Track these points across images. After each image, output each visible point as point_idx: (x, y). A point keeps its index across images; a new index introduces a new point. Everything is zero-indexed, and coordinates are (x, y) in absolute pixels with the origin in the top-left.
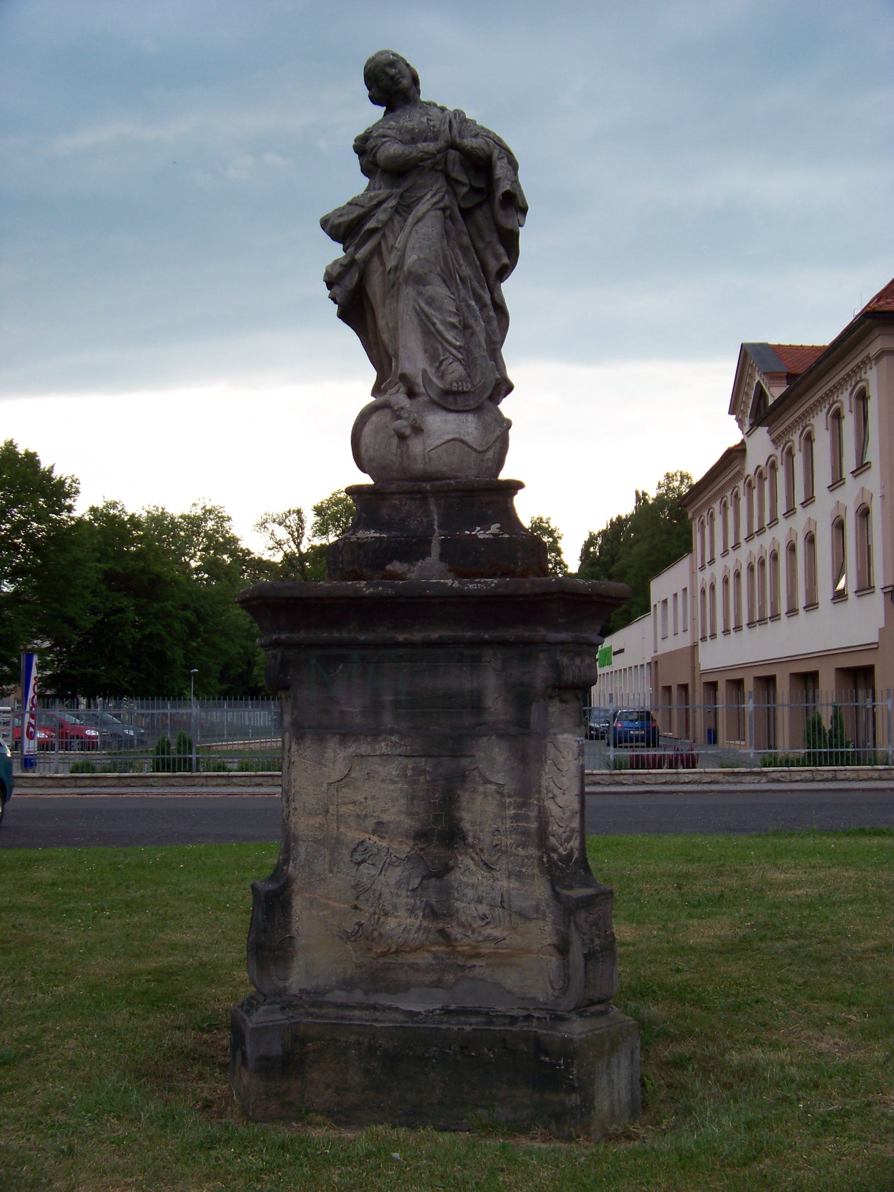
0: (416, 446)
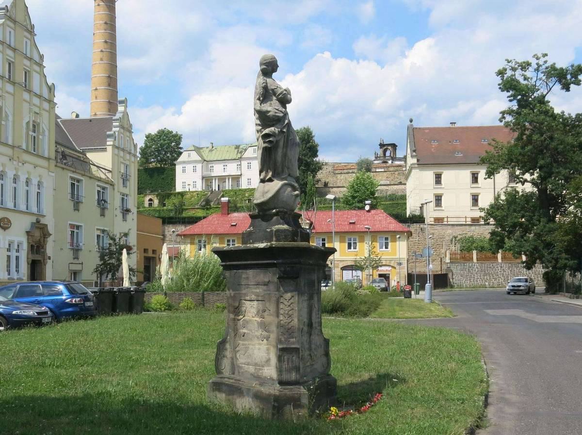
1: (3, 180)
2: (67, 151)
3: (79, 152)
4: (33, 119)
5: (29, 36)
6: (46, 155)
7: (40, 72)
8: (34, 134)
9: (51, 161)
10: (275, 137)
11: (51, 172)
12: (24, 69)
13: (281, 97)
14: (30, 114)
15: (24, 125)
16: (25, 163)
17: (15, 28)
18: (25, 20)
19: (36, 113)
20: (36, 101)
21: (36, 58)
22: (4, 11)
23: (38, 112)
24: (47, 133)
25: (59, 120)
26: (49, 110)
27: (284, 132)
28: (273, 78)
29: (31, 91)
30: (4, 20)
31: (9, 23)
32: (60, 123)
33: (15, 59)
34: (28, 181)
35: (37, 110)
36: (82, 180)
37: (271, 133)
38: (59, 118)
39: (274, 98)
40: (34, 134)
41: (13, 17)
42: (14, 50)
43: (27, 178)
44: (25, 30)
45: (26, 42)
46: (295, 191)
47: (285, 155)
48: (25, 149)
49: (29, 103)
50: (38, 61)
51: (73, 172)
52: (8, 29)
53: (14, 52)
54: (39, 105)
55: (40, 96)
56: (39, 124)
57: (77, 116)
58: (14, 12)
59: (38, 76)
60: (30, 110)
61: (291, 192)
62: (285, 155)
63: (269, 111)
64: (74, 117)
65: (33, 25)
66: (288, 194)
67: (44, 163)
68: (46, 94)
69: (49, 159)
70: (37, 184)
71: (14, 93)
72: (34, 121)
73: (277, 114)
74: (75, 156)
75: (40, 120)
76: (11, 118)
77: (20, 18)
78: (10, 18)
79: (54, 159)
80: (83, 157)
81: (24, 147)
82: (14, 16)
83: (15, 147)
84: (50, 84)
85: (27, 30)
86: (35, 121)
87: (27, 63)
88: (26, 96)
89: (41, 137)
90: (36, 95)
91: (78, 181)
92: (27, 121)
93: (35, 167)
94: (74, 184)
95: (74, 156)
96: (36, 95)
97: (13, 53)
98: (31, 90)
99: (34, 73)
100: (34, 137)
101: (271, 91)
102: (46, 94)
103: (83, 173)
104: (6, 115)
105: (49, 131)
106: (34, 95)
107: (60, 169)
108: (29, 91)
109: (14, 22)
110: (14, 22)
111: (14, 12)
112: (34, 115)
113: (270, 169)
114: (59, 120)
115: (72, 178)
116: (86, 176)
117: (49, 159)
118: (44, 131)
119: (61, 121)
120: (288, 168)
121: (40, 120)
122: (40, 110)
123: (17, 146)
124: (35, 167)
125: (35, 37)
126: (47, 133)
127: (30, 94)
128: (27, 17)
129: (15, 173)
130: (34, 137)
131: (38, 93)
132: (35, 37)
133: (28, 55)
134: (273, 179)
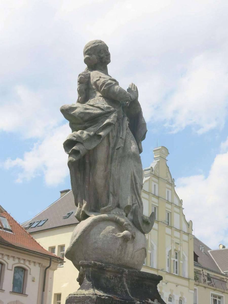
0: (130, 247)
1: (171, 301)
2: (212, 274)
3: (222, 274)
4: (175, 248)
5: (170, 187)
6: (187, 276)
7: (180, 212)
8: (176, 260)
9: (190, 281)
10: (82, 143)
11: (191, 290)
12: (166, 210)
13: (104, 89)
14: (171, 244)
15: (167, 254)
16: (168, 283)
17: (159, 182)
18: (167, 177)
19: (176, 243)
20: (177, 234)
21: (176, 202)
22: (150, 171)
23: (179, 243)
24: (186, 259)
25: (209, 251)
26: (189, 241)
27: (100, 136)
28: (109, 74)
29: (172, 227)
30: (149, 177)
31: (154, 179)
32: (210, 254)
33: (158, 204)
34: (171, 297)
35: (178, 241)
36: (222, 297)
37: (75, 139)
38: (210, 249)
39: (99, 94)
40: (176, 260)
41: (157, 174)
42: (158, 197)
43: (180, 298)
44: (167, 183)
45: (168, 192)
46: (122, 231)
47: (108, 176)
48: (168, 272)
49: (171, 236)
50: (178, 205)
51: (215, 290)
52: (153, 184)
53: (158, 199)
54: (170, 233)
55: (180, 231)
56: (179, 252)
57: (224, 247)
58: (158, 171)
59: (179, 215)
60: (172, 241)
61: (113, 231)
62: (108, 176)
63: (76, 108)
64: (221, 247)
65: (173, 179)
66: (105, 236)
67: (185, 282)
68: (185, 229)
69: (189, 279)
70: (179, 300)
71: (158, 229)
72: (175, 250)
73: (87, 111)
74: (219, 278)
75: (180, 248)
76: (155, 248)
77: (162, 174)
78: (155, 176)
79: (194, 279)
80: (226, 279)
81: (167, 269)
82: (158, 174)
83: (159, 270)
84: (188, 220)
85: (168, 183)
86: (177, 249)
87: (169, 206)
88: (168, 231)
89: (181, 262)
90: (176, 230)
91: (220, 298)
92: (169, 250)
93: (177, 286)
94: (216, 300)
95: (217, 278)
96: (176, 230)
97: (157, 200)
98: (172, 226)
99: (175, 213)
100: (176, 262)
101: (94, 87)
102: (185, 229)
103: (223, 290)
104: (151, 246)
105: (189, 257)
106: (175, 230)
107: (203, 288)
108: (171, 227)
109: (158, 178)
110: (158, 178)
111: (158, 171)
112: (175, 245)
113: (85, 200)
114: (209, 251)
115: (214, 296)
116: (226, 293)
117: (189, 279)
118: (184, 257)
119: (210, 252)
120: (115, 195)
121: (180, 248)
122: (180, 241)
123: (161, 269)
124: (177, 286)
125: (175, 187)
126: (186, 259)
127: (171, 229)
128: (168, 174)
129: (180, 296)
130: (176, 262)
131: (178, 228)
132: (175, 187)
133: (170, 201)
134: (88, 213)
